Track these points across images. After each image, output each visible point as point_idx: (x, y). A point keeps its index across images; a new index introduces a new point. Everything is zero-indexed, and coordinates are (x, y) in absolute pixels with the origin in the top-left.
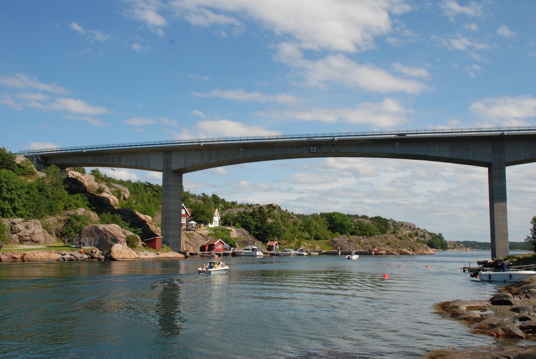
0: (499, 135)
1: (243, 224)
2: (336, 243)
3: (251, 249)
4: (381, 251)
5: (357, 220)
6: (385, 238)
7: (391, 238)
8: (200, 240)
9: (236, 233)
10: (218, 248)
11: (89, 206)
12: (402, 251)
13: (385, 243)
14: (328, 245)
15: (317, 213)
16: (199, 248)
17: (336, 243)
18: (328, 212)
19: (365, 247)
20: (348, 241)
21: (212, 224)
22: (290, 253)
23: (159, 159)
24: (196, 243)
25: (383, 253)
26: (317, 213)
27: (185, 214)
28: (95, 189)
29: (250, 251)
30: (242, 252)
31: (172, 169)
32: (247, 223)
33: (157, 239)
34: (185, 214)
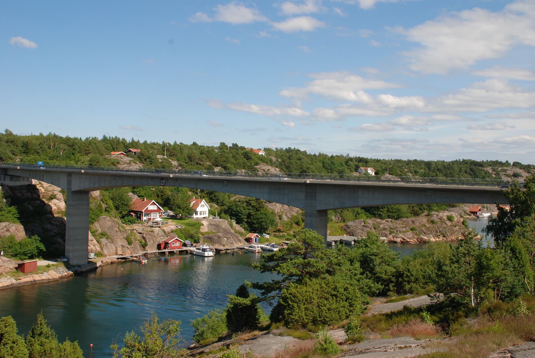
0: (303, 182)
1: (234, 213)
2: (349, 228)
3: (201, 249)
4: (396, 238)
5: (501, 168)
6: (413, 222)
7: (420, 222)
8: (160, 237)
9: (207, 228)
10: (174, 245)
11: (18, 218)
12: (422, 239)
13: (409, 228)
14: (341, 230)
15: (459, 159)
16: (156, 245)
17: (349, 228)
18: (469, 158)
19: (381, 233)
20: (363, 226)
21: (197, 215)
22: (255, 249)
23: (64, 179)
24: (153, 241)
25: (397, 241)
26: (459, 159)
27: (157, 209)
28: (48, 195)
29: (201, 251)
30: (194, 251)
31: (72, 190)
32: (238, 212)
33: (25, 264)
34: (157, 209)
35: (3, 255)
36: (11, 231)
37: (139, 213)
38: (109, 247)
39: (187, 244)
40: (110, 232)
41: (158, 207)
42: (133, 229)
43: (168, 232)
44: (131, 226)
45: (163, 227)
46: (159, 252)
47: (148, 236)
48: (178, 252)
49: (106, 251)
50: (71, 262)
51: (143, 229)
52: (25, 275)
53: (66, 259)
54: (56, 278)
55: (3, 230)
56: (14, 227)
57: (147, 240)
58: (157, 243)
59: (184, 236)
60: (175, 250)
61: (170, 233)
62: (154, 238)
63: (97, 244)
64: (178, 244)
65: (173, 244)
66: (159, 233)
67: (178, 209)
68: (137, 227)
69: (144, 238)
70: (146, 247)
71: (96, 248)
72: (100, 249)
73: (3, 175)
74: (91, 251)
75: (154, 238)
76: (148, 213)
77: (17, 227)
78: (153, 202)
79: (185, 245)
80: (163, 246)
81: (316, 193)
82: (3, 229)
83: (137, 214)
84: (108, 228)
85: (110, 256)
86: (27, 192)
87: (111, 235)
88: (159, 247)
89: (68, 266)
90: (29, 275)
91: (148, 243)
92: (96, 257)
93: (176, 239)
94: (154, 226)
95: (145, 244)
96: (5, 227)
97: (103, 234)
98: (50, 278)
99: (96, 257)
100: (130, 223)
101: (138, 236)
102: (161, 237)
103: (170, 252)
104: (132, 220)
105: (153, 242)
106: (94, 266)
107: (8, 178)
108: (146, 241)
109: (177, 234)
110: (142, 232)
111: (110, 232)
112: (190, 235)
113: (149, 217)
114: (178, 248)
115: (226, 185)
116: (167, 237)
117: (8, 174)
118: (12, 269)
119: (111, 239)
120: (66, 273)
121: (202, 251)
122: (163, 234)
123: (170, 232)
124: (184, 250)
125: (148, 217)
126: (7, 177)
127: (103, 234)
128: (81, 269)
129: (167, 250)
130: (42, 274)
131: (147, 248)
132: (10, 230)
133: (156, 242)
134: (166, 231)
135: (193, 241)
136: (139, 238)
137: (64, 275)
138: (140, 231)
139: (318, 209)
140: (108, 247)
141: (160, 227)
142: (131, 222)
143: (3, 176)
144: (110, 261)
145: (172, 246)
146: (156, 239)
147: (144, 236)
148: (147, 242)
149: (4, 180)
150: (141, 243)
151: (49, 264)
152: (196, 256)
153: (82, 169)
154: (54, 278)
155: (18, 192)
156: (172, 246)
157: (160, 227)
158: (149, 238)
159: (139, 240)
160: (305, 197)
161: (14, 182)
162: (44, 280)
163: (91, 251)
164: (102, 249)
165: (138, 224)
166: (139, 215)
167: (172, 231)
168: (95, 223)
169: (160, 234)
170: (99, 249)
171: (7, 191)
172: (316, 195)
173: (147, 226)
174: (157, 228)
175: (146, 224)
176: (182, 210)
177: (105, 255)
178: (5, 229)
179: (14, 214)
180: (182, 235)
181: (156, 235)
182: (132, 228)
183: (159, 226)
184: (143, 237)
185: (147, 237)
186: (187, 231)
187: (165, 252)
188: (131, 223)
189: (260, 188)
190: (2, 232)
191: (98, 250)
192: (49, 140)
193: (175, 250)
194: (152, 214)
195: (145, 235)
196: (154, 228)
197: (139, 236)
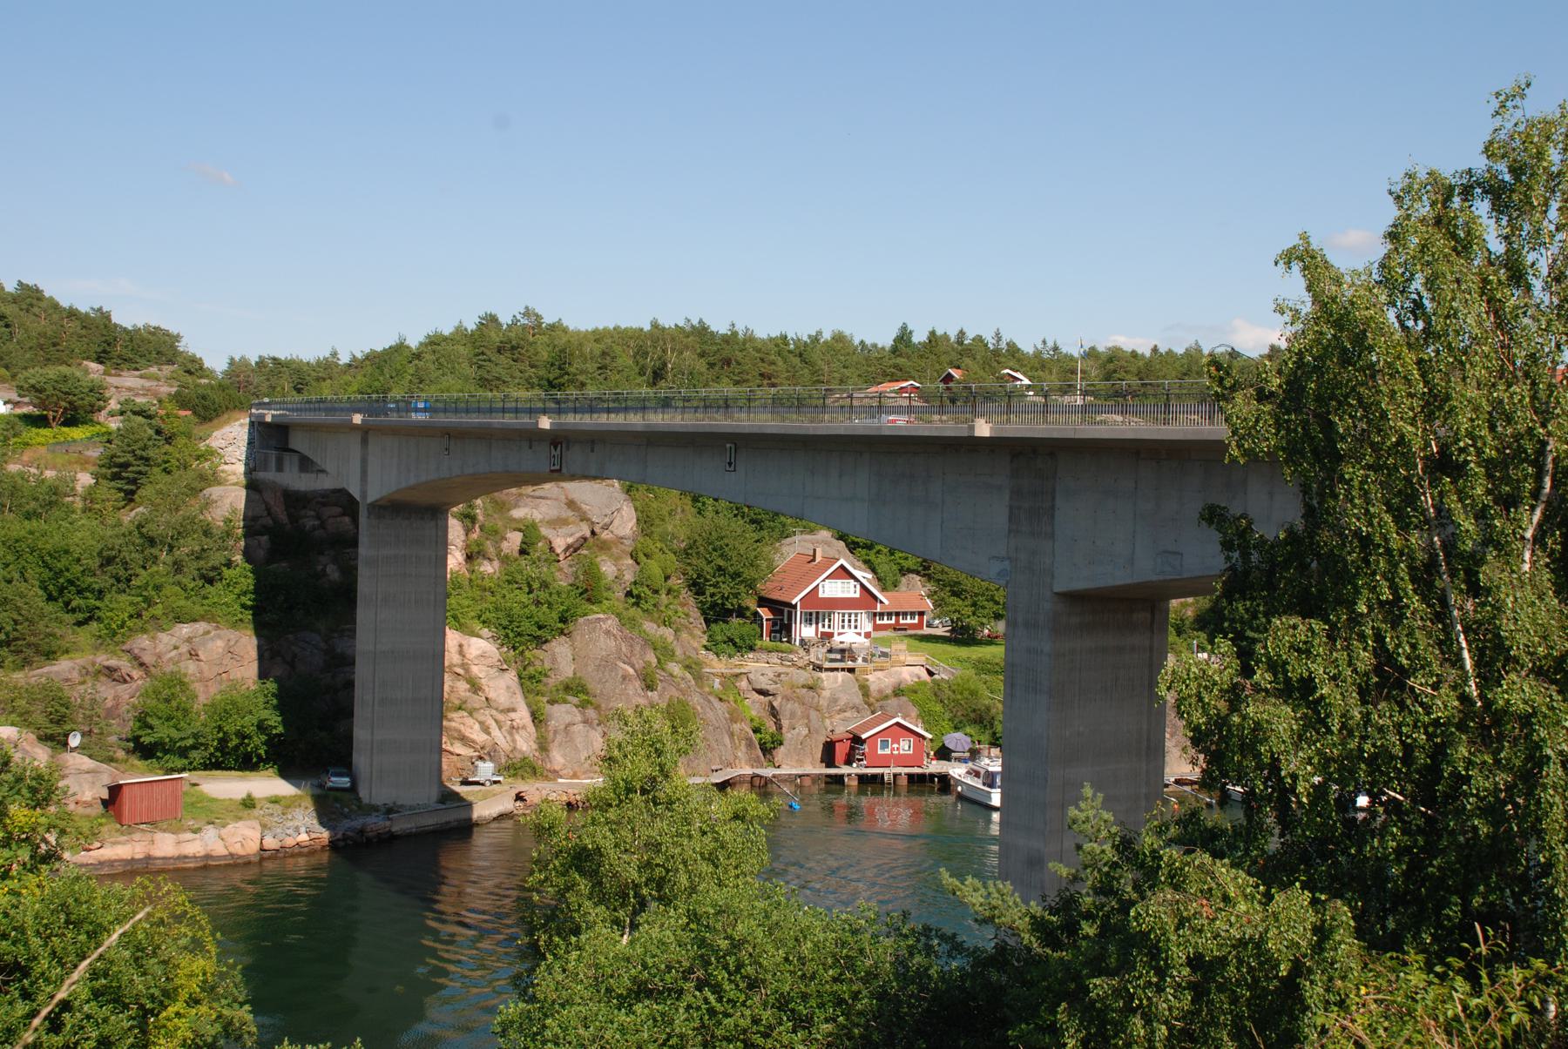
3: (982, 772)
10: (888, 751)
24: (807, 726)
33: (126, 790)
34: (857, 595)
35: (81, 749)
36: (202, 657)
37: (786, 609)
38: (579, 740)
39: (951, 746)
40: (600, 681)
41: (862, 586)
42: (737, 675)
43: (880, 691)
44: (736, 660)
45: (865, 672)
46: (828, 776)
47: (789, 706)
48: (903, 781)
49: (564, 756)
50: (363, 793)
51: (779, 675)
52: (122, 834)
53: (347, 779)
54: (241, 852)
55: (174, 653)
56: (220, 643)
57: (785, 723)
58: (823, 739)
59: (947, 715)
60: (886, 771)
61: (886, 697)
62: (813, 714)
63: (524, 727)
64: (905, 746)
65: (885, 744)
66: (841, 695)
67: (952, 599)
68: (759, 667)
69: (774, 712)
70: (774, 752)
71: (514, 741)
72: (535, 746)
73: (277, 449)
74: (489, 754)
75: (813, 714)
76: (819, 610)
77: (232, 643)
78: (842, 567)
79: (944, 754)
80: (841, 751)
81: (1053, 499)
82: (176, 648)
83: (782, 613)
84: (597, 662)
85: (575, 776)
86: (344, 514)
87: (602, 693)
88: (828, 756)
89: (326, 807)
90: (137, 836)
91: (788, 735)
92: (501, 779)
93: (898, 724)
94: (827, 665)
95: (772, 736)
96: (189, 640)
97: (574, 688)
98: (214, 854)
99: (501, 779)
100: (731, 649)
101: (753, 702)
102: (848, 714)
103: (863, 779)
104: (742, 638)
105: (805, 731)
106: (462, 815)
107: (291, 463)
108: (779, 727)
109: (915, 703)
110: (771, 688)
111: (600, 681)
112: (974, 711)
113: (826, 630)
114: (902, 761)
115: (730, 464)
116: (873, 713)
117: (291, 446)
118: (88, 805)
119: (597, 708)
120: (303, 837)
121: (984, 784)
122: (858, 699)
123: (889, 691)
124: (932, 776)
125: (821, 629)
126: (287, 457)
127: (574, 688)
128: (388, 823)
129: (854, 769)
130: (195, 832)
131: (780, 753)
132: (200, 653)
133: (817, 732)
134: (873, 688)
135: (986, 737)
136: (754, 713)
137: (290, 842)
138: (764, 684)
139: (1060, 587)
140: (572, 740)
141: (851, 670)
142: (735, 644)
143: (273, 454)
144: (565, 798)
145: (880, 752)
146: (823, 718)
147: (775, 704)
148: (784, 730)
149: (280, 468)
150: (756, 730)
151: (249, 796)
152: (967, 806)
153: (358, 411)
154: (231, 855)
155: (312, 513)
156: (880, 752)
157: (851, 670)
158: (793, 715)
159: (752, 720)
160: (1010, 520)
161: (314, 475)
162: (186, 857)
163: (489, 754)
164: (543, 747)
165: (764, 656)
166: (782, 618)
167: (898, 692)
168: (554, 643)
169: (844, 699)
170: (525, 744)
171: (268, 510)
172: (1053, 508)
173: (800, 664)
174: (840, 675)
175: (801, 657)
176: (969, 602)
177: (555, 772)
178: (184, 649)
179: (245, 593)
180: (938, 708)
181: (823, 703)
182: (737, 671)
183: (850, 664)
184: (773, 707)
185: (787, 709)
186: (966, 693)
187: (842, 776)
188: (739, 648)
189: (840, 476)
190: (171, 659)
191: (520, 751)
192: (661, 343)
193: (888, 772)
194: (837, 617)
195: (779, 699)
196: (824, 675)
197: (757, 705)
